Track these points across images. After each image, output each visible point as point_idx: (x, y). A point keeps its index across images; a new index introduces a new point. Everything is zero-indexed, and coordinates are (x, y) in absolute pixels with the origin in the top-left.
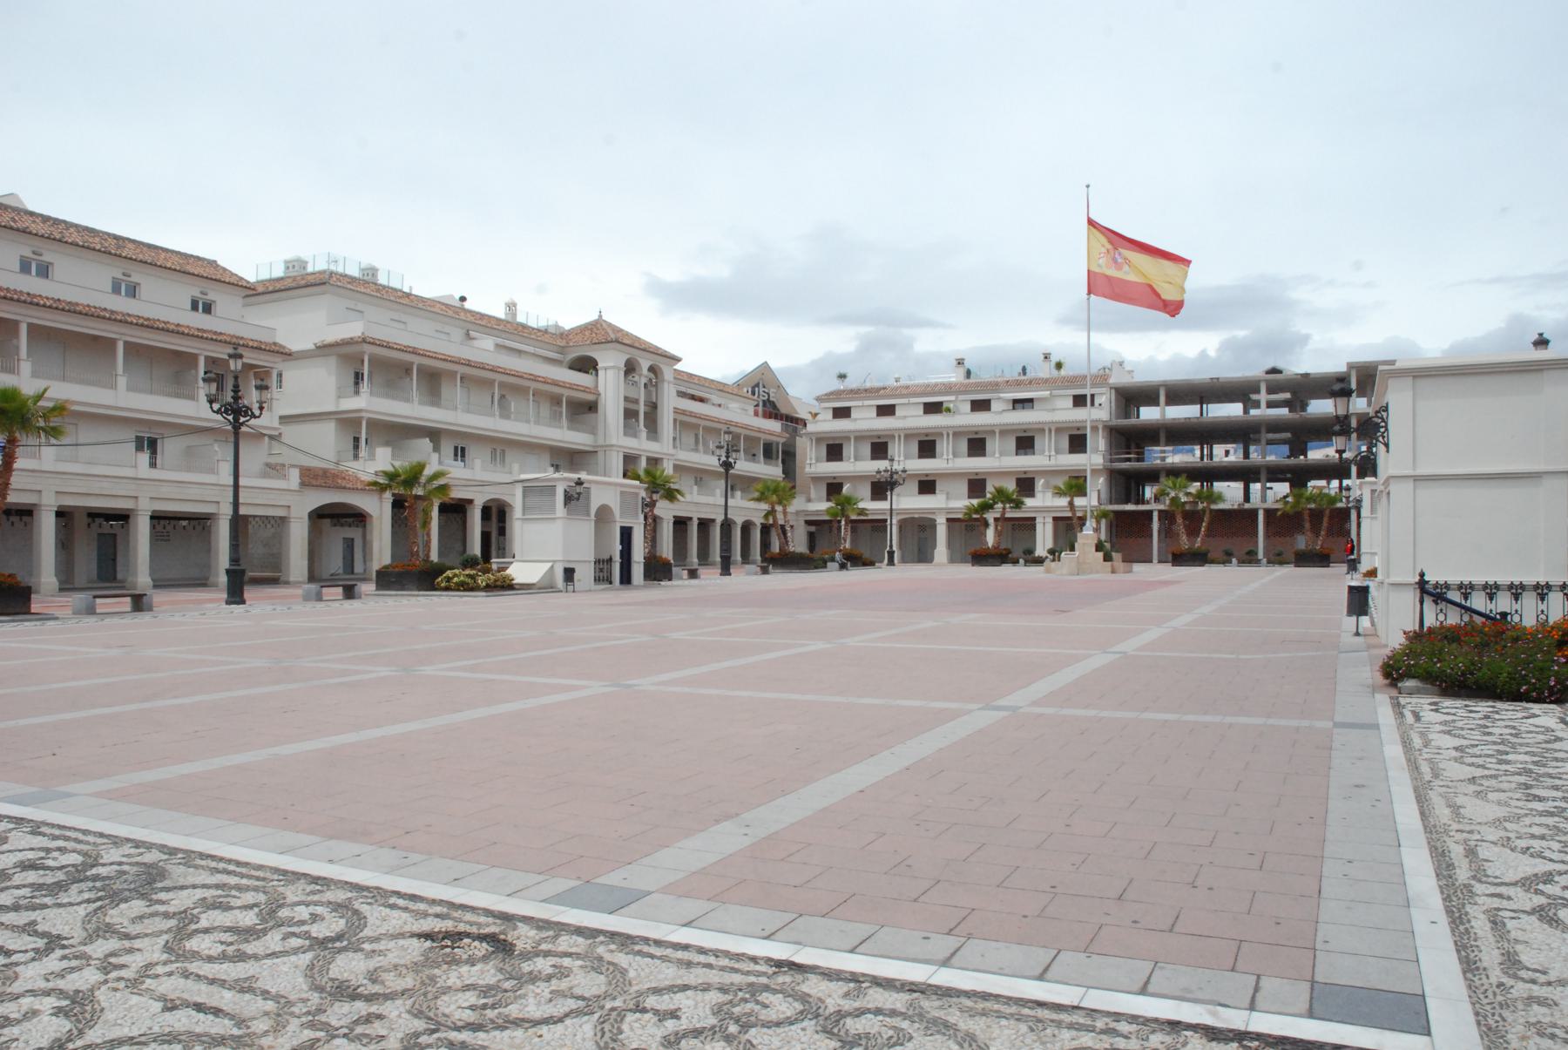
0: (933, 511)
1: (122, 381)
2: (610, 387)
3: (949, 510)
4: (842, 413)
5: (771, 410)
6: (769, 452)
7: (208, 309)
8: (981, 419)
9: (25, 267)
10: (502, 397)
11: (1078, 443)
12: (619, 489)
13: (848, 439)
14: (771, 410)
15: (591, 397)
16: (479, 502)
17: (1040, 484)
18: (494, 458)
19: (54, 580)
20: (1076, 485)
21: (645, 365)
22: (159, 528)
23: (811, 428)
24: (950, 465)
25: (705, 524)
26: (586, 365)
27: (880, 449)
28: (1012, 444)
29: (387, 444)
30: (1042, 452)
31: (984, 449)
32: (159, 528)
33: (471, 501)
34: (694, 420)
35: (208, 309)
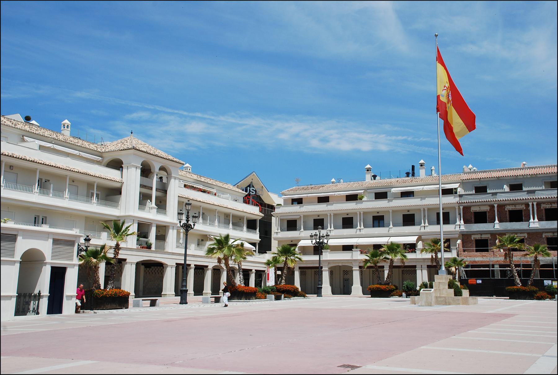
5: (258, 201)
6: (251, 225)
10: (203, 214)
14: (258, 201)
18: (198, 245)
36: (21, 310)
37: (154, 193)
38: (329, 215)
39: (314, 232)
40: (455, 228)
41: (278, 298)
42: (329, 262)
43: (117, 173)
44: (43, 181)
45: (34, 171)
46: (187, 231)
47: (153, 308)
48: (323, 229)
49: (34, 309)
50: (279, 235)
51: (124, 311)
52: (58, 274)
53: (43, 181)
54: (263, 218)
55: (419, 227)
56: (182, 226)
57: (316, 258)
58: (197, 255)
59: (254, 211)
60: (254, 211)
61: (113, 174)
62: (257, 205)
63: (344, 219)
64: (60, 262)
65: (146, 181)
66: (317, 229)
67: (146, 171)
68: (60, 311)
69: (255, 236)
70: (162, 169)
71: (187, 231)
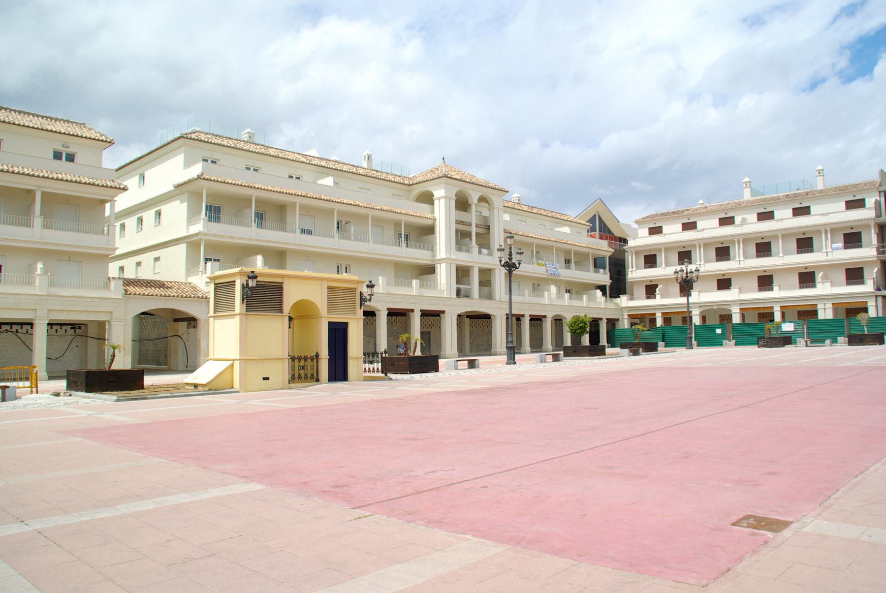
0: (729, 303)
1: (38, 221)
2: (442, 214)
3: (742, 302)
4: (656, 231)
5: (605, 232)
6: (598, 264)
7: (71, 158)
8: (767, 226)
9: (57, 156)
10: (538, 252)
11: (852, 239)
12: (325, 285)
13: (660, 250)
14: (605, 232)
15: (429, 222)
16: (550, 316)
17: (819, 277)
18: (534, 289)
19: (46, 374)
20: (854, 275)
21: (474, 198)
22: (53, 332)
23: (631, 243)
24: (742, 265)
25: (537, 320)
26: (427, 198)
27: (685, 256)
28: (794, 245)
29: (417, 278)
30: (820, 250)
31: (770, 250)
32: (53, 332)
33: (545, 317)
34: (528, 240)
35: (71, 158)
36: (296, 375)
37: (474, 230)
38: (736, 240)
39: (679, 268)
40: (122, 269)
41: (636, 353)
42: (700, 305)
43: (426, 207)
44: (344, 223)
45: (330, 212)
46: (510, 272)
47: (473, 371)
48: (690, 263)
49: (312, 375)
50: (636, 273)
51: (430, 375)
52: (338, 333)
53: (344, 223)
54: (614, 253)
55: (776, 258)
56: (503, 266)
57: (684, 300)
58: (527, 303)
59: (604, 248)
60: (604, 248)
61: (422, 209)
62: (606, 239)
63: (799, 241)
64: (338, 318)
65: (463, 216)
66: (683, 264)
67: (462, 204)
68: (345, 378)
69: (604, 278)
70: (482, 199)
71: (510, 272)
